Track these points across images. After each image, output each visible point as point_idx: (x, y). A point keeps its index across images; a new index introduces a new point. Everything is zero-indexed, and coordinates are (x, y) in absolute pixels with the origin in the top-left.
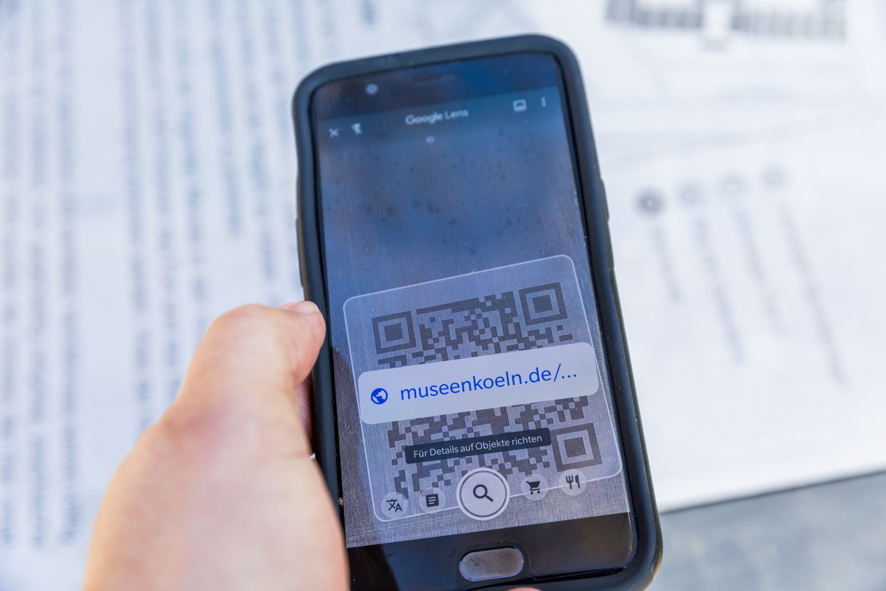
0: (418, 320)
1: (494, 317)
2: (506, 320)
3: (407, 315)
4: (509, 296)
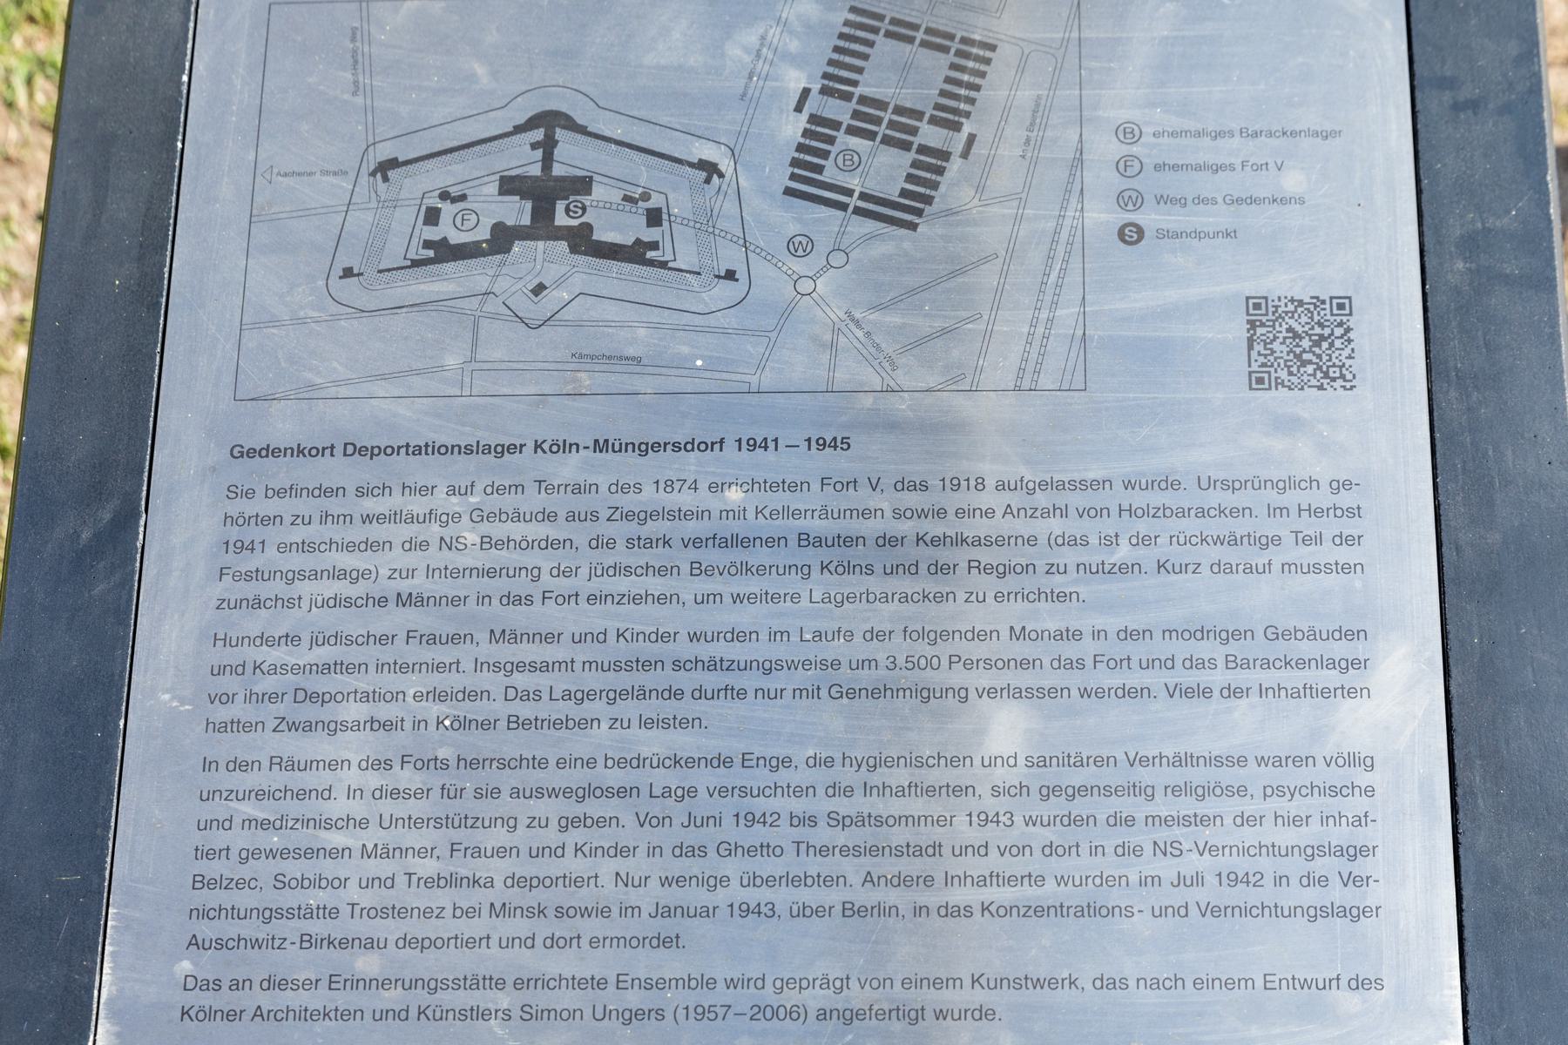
0: (1255, 367)
1: (1260, 331)
2: (1263, 325)
3: (1250, 373)
4: (1248, 322)
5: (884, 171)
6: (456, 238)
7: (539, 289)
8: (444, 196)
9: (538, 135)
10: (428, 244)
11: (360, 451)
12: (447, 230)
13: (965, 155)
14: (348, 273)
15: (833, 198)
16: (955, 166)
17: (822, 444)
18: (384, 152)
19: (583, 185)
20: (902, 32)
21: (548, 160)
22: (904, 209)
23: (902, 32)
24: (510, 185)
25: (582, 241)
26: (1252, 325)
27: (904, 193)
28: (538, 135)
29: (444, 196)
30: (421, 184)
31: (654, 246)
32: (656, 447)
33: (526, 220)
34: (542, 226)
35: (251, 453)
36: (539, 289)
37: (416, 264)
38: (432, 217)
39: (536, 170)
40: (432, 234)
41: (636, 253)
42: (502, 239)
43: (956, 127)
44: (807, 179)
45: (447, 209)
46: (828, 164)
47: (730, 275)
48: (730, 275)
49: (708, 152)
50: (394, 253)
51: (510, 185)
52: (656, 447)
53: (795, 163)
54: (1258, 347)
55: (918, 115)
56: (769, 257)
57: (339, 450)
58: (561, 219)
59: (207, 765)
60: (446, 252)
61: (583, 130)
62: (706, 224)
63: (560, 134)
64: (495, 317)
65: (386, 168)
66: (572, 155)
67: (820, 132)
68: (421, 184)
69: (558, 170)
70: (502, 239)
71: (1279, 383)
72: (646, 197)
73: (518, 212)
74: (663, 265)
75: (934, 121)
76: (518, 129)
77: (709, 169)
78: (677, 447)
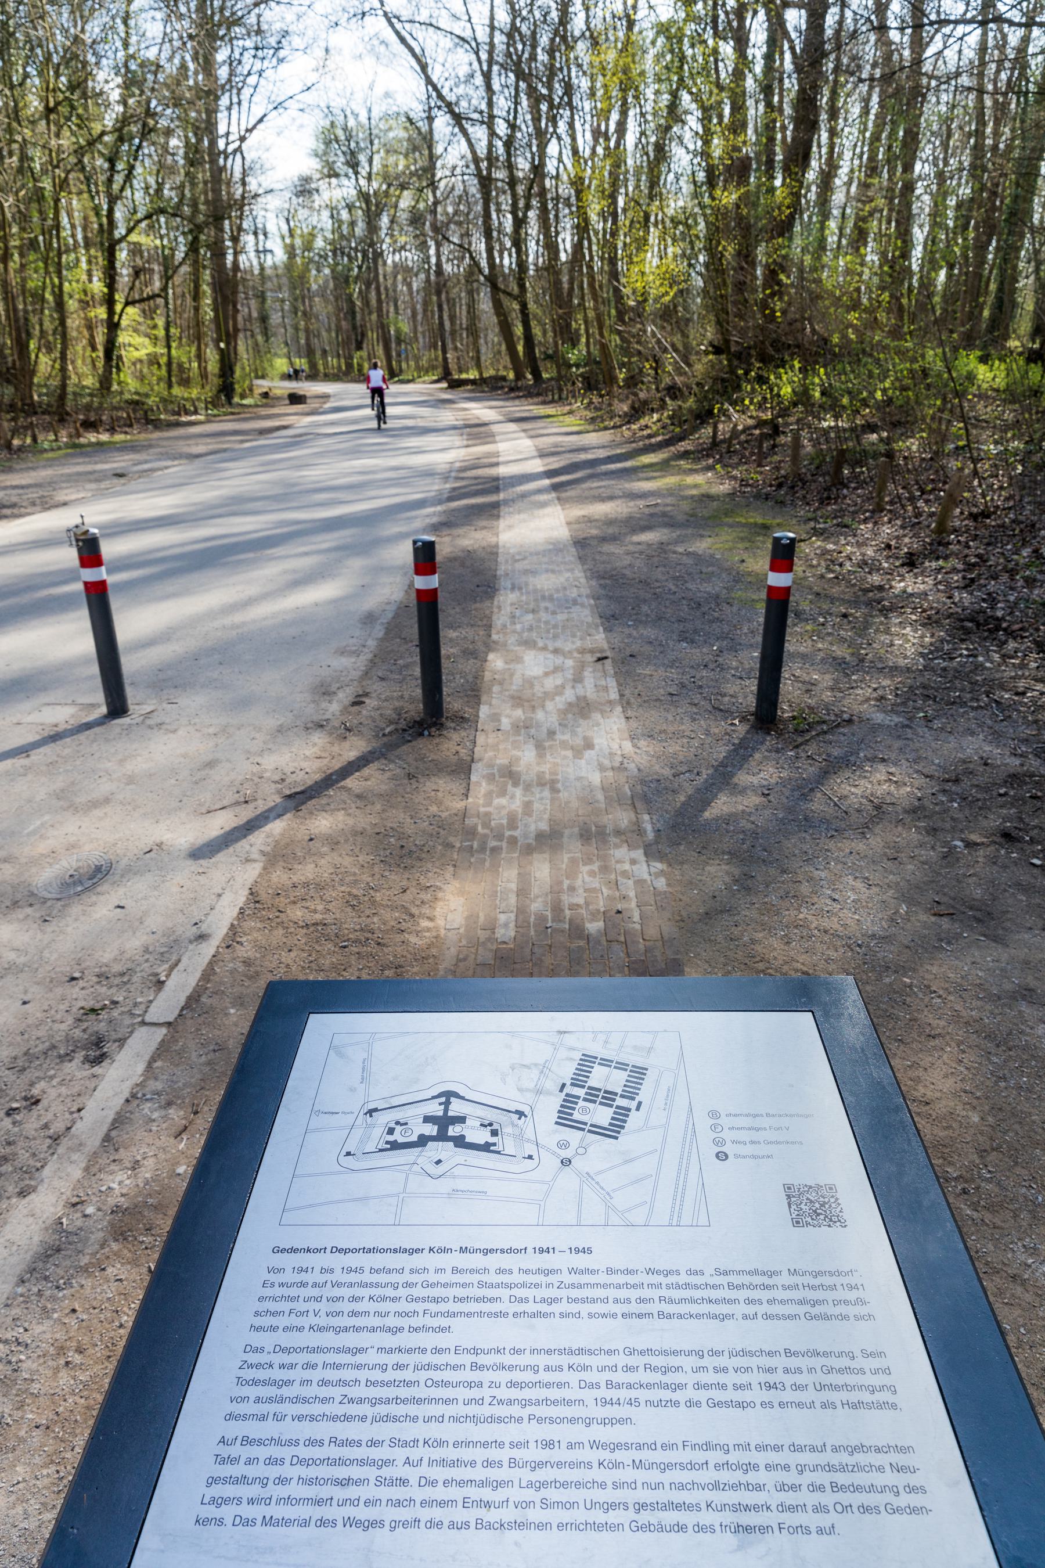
5: (603, 1116)
6: (401, 1140)
7: (439, 1162)
8: (397, 1123)
9: (443, 1099)
10: (387, 1143)
11: (340, 1251)
12: (398, 1137)
13: (638, 1109)
14: (348, 1154)
15: (578, 1126)
16: (633, 1113)
17: (578, 1251)
18: (371, 1106)
19: (462, 1120)
20: (606, 1062)
21: (446, 1110)
22: (613, 1130)
23: (606, 1062)
24: (427, 1119)
25: (460, 1142)
26: (789, 1197)
27: (611, 1124)
28: (443, 1099)
29: (397, 1123)
30: (384, 1119)
31: (494, 1144)
32: (491, 1251)
33: (435, 1133)
34: (442, 1136)
35: (283, 1251)
36: (439, 1162)
37: (381, 1150)
38: (391, 1131)
39: (441, 1113)
40: (391, 1138)
41: (486, 1147)
42: (423, 1141)
43: (633, 1099)
44: (565, 1118)
45: (398, 1128)
46: (575, 1113)
47: (530, 1157)
48: (530, 1157)
49: (521, 1108)
50: (371, 1147)
51: (427, 1119)
52: (491, 1251)
53: (559, 1112)
54: (793, 1207)
55: (616, 1094)
56: (548, 1150)
57: (328, 1250)
58: (451, 1133)
59: (223, 1441)
60: (395, 1146)
61: (463, 1098)
62: (520, 1138)
63: (452, 1099)
64: (416, 1173)
65: (371, 1112)
66: (456, 1108)
67: (570, 1101)
68: (384, 1119)
69: (450, 1114)
70: (423, 1141)
71: (808, 1224)
72: (491, 1125)
73: (431, 1130)
74: (498, 1153)
75: (622, 1096)
76: (434, 1098)
77: (521, 1114)
78: (502, 1251)
